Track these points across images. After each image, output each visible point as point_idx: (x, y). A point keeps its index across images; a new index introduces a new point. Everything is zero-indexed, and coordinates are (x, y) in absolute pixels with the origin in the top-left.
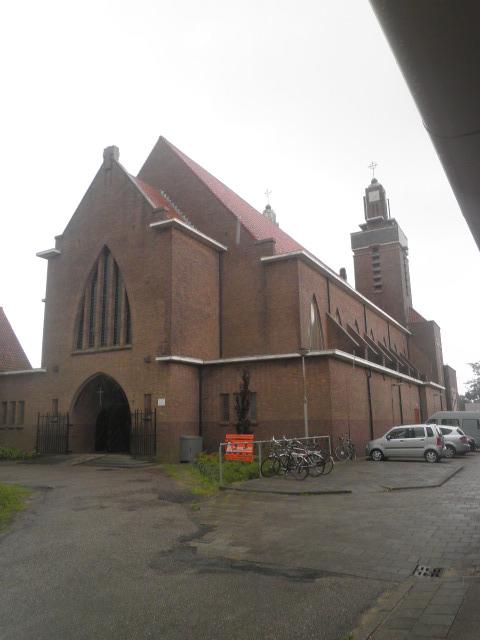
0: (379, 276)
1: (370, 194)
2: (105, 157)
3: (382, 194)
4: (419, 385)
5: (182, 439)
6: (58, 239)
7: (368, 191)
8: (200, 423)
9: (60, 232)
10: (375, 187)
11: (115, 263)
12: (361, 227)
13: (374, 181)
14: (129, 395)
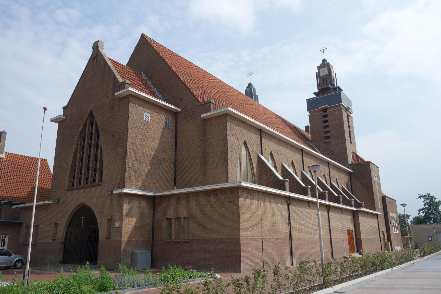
0: (328, 129)
1: (321, 70)
2: (93, 49)
3: (330, 70)
4: (353, 212)
5: (133, 253)
6: (64, 108)
7: (319, 68)
8: (153, 240)
9: (66, 104)
10: (325, 64)
11: (96, 121)
12: (315, 94)
13: (324, 61)
14: (99, 219)
